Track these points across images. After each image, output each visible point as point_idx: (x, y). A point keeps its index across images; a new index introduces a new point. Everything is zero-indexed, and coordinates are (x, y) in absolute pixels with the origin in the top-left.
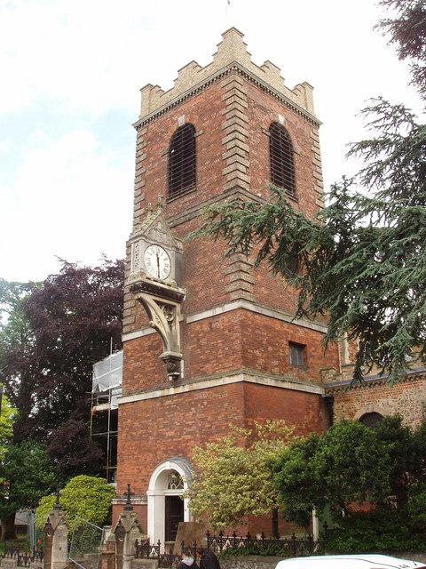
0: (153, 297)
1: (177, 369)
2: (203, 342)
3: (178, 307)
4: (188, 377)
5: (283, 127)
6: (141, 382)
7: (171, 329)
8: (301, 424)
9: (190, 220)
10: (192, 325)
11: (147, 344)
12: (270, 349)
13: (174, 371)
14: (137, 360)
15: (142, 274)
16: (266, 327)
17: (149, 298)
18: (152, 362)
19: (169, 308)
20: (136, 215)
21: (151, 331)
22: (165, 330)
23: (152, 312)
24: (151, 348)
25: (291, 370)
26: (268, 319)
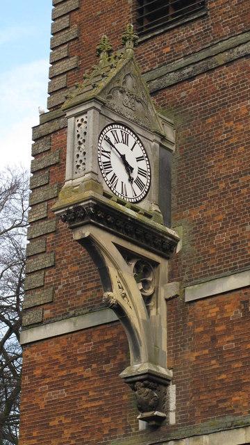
0: (114, 239)
1: (161, 404)
2: (226, 343)
3: (164, 266)
4: (187, 419)
6: (67, 433)
7: (149, 313)
9: (192, 78)
10: (197, 306)
11: (83, 349)
13: (154, 408)
14: (54, 386)
15: (95, 184)
17: (106, 240)
18: (95, 389)
19: (144, 269)
20: (57, 72)
21: (111, 316)
22: (136, 313)
23: (113, 273)
24: (91, 358)
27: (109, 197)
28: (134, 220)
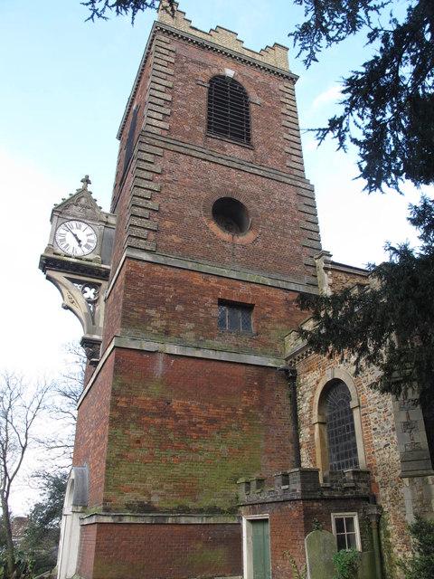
5: (233, 80)
8: (234, 409)
12: (179, 308)
16: (175, 281)
25: (220, 335)
26: (179, 271)
27: (60, 255)
28: (74, 264)
